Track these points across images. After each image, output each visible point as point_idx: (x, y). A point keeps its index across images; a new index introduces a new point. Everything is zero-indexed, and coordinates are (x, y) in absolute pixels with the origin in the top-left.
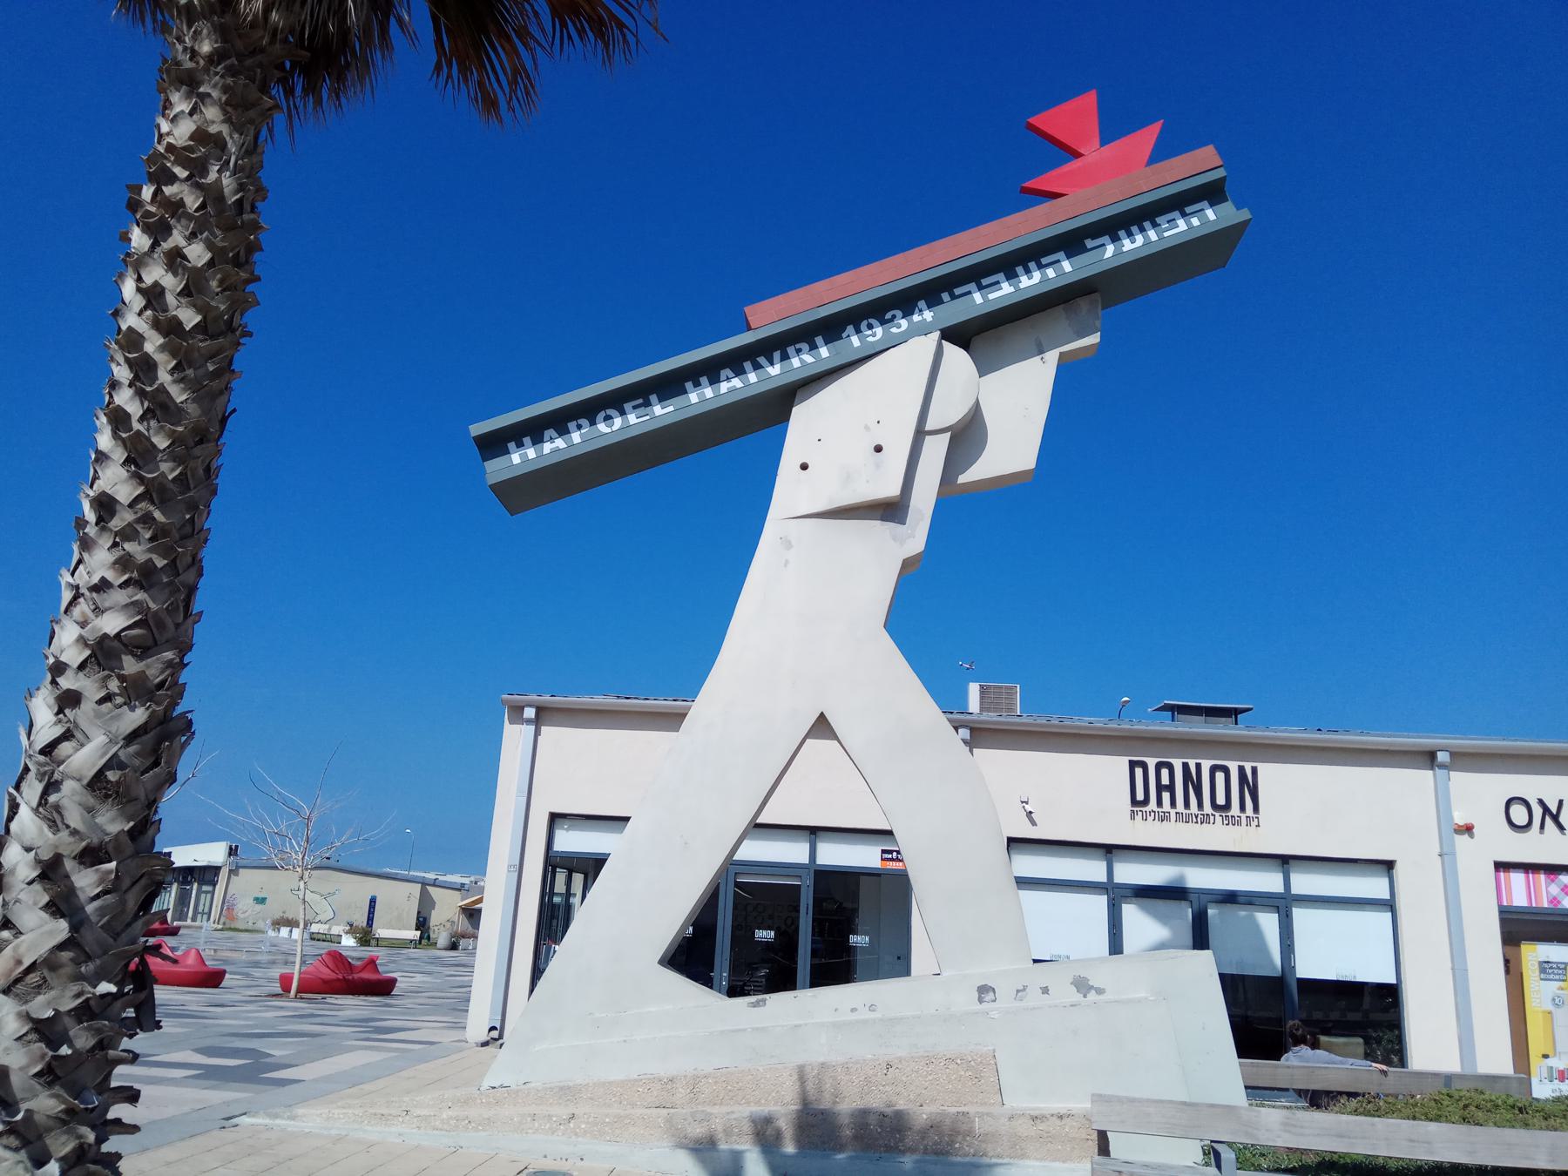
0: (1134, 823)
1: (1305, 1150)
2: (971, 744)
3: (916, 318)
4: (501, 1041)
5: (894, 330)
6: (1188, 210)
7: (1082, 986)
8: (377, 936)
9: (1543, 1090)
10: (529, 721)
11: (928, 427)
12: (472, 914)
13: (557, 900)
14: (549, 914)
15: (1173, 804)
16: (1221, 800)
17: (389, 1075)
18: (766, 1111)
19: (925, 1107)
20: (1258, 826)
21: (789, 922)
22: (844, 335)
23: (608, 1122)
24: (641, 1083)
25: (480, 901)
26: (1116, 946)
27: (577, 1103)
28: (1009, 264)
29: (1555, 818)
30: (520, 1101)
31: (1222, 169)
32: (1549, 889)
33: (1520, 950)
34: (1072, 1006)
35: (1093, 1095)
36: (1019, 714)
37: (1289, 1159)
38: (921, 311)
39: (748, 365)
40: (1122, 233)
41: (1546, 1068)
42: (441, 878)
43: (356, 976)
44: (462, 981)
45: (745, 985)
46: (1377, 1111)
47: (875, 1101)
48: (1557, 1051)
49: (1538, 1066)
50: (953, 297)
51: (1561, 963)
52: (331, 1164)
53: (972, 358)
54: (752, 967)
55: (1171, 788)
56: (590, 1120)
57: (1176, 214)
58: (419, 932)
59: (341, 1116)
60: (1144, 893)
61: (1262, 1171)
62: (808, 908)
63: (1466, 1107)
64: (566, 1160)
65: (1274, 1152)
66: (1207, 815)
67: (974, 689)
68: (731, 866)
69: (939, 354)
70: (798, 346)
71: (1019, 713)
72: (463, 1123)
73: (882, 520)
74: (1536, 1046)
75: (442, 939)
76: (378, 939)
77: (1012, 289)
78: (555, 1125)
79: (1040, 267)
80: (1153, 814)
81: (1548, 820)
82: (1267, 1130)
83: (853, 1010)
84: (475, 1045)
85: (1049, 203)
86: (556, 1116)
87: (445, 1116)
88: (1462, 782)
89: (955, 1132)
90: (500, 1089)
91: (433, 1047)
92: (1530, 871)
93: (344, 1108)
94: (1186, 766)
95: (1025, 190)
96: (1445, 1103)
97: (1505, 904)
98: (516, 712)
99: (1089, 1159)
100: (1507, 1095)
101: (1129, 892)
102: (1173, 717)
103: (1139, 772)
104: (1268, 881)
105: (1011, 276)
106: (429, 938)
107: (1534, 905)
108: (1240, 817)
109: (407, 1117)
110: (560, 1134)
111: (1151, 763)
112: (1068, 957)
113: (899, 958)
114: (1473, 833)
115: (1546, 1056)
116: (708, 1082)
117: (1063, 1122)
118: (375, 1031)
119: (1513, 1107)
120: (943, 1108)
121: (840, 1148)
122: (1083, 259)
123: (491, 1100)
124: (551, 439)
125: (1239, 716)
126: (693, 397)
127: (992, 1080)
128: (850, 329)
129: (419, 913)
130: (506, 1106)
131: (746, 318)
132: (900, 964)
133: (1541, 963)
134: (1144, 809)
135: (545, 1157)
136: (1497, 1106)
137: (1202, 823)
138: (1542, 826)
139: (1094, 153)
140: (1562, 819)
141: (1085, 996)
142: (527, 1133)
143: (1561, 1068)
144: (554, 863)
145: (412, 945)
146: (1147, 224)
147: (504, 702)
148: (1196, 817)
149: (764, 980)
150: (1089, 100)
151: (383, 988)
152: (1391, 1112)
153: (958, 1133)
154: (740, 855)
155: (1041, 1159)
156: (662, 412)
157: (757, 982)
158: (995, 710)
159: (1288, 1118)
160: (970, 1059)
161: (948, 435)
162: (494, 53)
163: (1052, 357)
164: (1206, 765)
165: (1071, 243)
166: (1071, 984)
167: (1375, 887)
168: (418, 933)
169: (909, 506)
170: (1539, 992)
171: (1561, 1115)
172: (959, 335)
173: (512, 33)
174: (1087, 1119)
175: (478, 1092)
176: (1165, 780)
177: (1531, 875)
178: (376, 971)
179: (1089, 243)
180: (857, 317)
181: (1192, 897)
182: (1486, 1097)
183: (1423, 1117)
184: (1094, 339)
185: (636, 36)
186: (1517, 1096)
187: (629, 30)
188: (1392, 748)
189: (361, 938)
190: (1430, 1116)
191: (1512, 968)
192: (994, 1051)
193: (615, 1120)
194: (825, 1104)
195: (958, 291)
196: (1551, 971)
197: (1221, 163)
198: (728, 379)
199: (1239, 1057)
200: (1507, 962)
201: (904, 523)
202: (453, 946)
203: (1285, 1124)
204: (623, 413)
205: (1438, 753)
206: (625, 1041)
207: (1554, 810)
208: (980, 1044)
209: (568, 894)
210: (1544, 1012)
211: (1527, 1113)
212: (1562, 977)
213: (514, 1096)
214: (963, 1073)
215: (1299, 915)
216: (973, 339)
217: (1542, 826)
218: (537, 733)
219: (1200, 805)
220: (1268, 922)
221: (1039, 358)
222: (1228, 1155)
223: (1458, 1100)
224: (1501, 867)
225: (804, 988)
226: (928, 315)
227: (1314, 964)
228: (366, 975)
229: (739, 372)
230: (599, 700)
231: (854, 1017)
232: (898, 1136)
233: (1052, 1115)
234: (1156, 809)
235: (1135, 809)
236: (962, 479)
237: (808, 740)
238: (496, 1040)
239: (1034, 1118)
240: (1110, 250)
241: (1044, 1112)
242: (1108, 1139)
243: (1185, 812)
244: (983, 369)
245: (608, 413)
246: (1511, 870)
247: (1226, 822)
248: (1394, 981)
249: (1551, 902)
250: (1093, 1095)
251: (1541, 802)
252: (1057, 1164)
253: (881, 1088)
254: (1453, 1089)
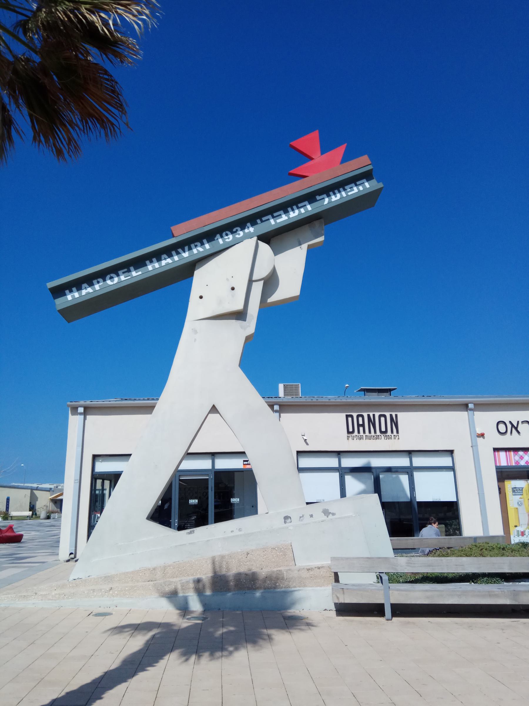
0: (349, 441)
1: (416, 573)
2: (280, 412)
3: (246, 231)
4: (75, 559)
5: (237, 236)
6: (358, 183)
7: (326, 512)
8: (11, 515)
9: (515, 539)
10: (81, 414)
11: (254, 278)
12: (58, 503)
13: (97, 492)
14: (94, 500)
15: (364, 432)
16: (383, 429)
17: (26, 578)
18: (196, 578)
19: (263, 569)
20: (399, 439)
21: (205, 494)
22: (216, 239)
23: (127, 590)
24: (141, 571)
25: (62, 494)
26: (343, 494)
27: (113, 583)
28: (285, 207)
29: (516, 429)
30: (87, 584)
31: (371, 165)
32: (515, 458)
33: (504, 484)
34: (322, 521)
35: (331, 558)
36: (300, 396)
37: (410, 577)
38: (248, 227)
39: (174, 253)
40: (331, 193)
41: (516, 531)
42: (40, 486)
43: (4, 535)
44: (54, 533)
45: (185, 524)
46: (447, 554)
47: (243, 569)
48: (520, 524)
49: (513, 531)
50: (262, 221)
51: (521, 488)
52: (3, 620)
53: (271, 248)
54: (189, 516)
55: (363, 425)
56: (119, 589)
57: (353, 185)
58: (31, 512)
59: (6, 598)
60: (354, 470)
61: (400, 583)
62: (212, 488)
63: (482, 549)
64: (110, 608)
65: (405, 575)
66: (378, 436)
67: (281, 387)
68: (178, 472)
69: (257, 246)
70: (196, 244)
71: (301, 398)
72: (62, 596)
73: (236, 319)
74: (512, 523)
75: (43, 515)
76: (11, 516)
77: (286, 218)
78: (103, 593)
79: (298, 208)
80: (356, 437)
81: (514, 430)
82: (401, 566)
83: (232, 531)
84: (63, 562)
85: (299, 181)
86: (104, 589)
87: (53, 594)
88: (479, 416)
89: (277, 579)
90: (77, 580)
91: (44, 564)
92: (507, 451)
93: (6, 594)
94: (369, 416)
95: (291, 174)
96: (474, 549)
97: (498, 465)
98: (74, 410)
99: (331, 584)
100: (498, 544)
101: (348, 471)
102: (365, 393)
103: (350, 419)
104: (403, 462)
105: (286, 212)
106: (36, 514)
107: (509, 465)
108: (391, 436)
109: (36, 596)
110: (106, 597)
111: (355, 415)
112: (324, 500)
113: (253, 507)
114: (484, 436)
115: (516, 526)
116: (170, 568)
117: (320, 570)
118: (16, 559)
119: (500, 548)
120: (271, 569)
121: (229, 590)
122: (316, 204)
123: (74, 585)
124: (86, 288)
125: (391, 392)
126: (150, 267)
127: (291, 555)
128: (218, 236)
129: (30, 503)
130: (81, 587)
131: (172, 232)
132: (253, 509)
133: (513, 488)
134: (352, 435)
135: (100, 607)
136: (493, 548)
137: (376, 439)
138: (511, 432)
139: (318, 158)
140: (519, 429)
141: (328, 517)
142: (91, 598)
143: (522, 531)
144: (95, 477)
145: (29, 518)
146: (341, 189)
147: (68, 406)
148: (374, 437)
149: (194, 521)
150: (315, 134)
151: (17, 539)
152: (453, 554)
153: (278, 579)
154: (181, 468)
155: (312, 587)
156: (136, 274)
157: (192, 522)
158: (291, 395)
159: (409, 561)
160: (281, 548)
161: (262, 282)
162: (60, 132)
163: (305, 246)
164: (377, 415)
165: (311, 197)
166: (322, 512)
167: (446, 461)
168: (31, 513)
169: (247, 313)
170: (512, 500)
171: (517, 551)
172: (265, 238)
173: (66, 123)
174: (330, 568)
175: (68, 582)
176: (361, 422)
177: (508, 453)
178: (13, 531)
179: (318, 198)
180: (221, 230)
181: (374, 471)
182: (490, 545)
183: (464, 555)
184: (321, 239)
185: (119, 129)
186: (503, 544)
187: (116, 126)
188: (450, 403)
189: (4, 517)
190: (467, 554)
191: (501, 491)
192: (291, 543)
193: (130, 588)
194: (224, 572)
195: (264, 219)
196: (517, 491)
197: (370, 163)
198: (165, 259)
199: (390, 537)
200: (499, 489)
201: (245, 321)
202: (48, 518)
203: (407, 563)
204: (118, 275)
205: (469, 404)
206: (133, 554)
207: (516, 426)
208: (285, 541)
209: (103, 489)
210: (514, 508)
211: (505, 550)
212: (521, 493)
213: (84, 582)
214: (278, 554)
215: (416, 475)
216: (272, 239)
217: (511, 432)
218: (85, 419)
219: (375, 432)
220: (404, 479)
221: (299, 247)
222: (385, 578)
223: (479, 547)
224: (496, 450)
225: (212, 523)
226: (252, 229)
227: (422, 496)
228: (9, 534)
229: (170, 256)
230: (112, 402)
231: (232, 534)
232: (252, 583)
233: (316, 568)
234: (357, 435)
235: (349, 435)
236: (270, 300)
237: (209, 415)
238: (73, 558)
239: (308, 570)
240: (327, 200)
241: (312, 567)
242: (338, 575)
243: (369, 435)
244: (276, 252)
245: (111, 276)
246: (500, 451)
247: (386, 438)
248: (455, 500)
249: (516, 463)
250: (331, 558)
251: (510, 422)
252: (318, 588)
253: (245, 563)
254: (477, 543)
